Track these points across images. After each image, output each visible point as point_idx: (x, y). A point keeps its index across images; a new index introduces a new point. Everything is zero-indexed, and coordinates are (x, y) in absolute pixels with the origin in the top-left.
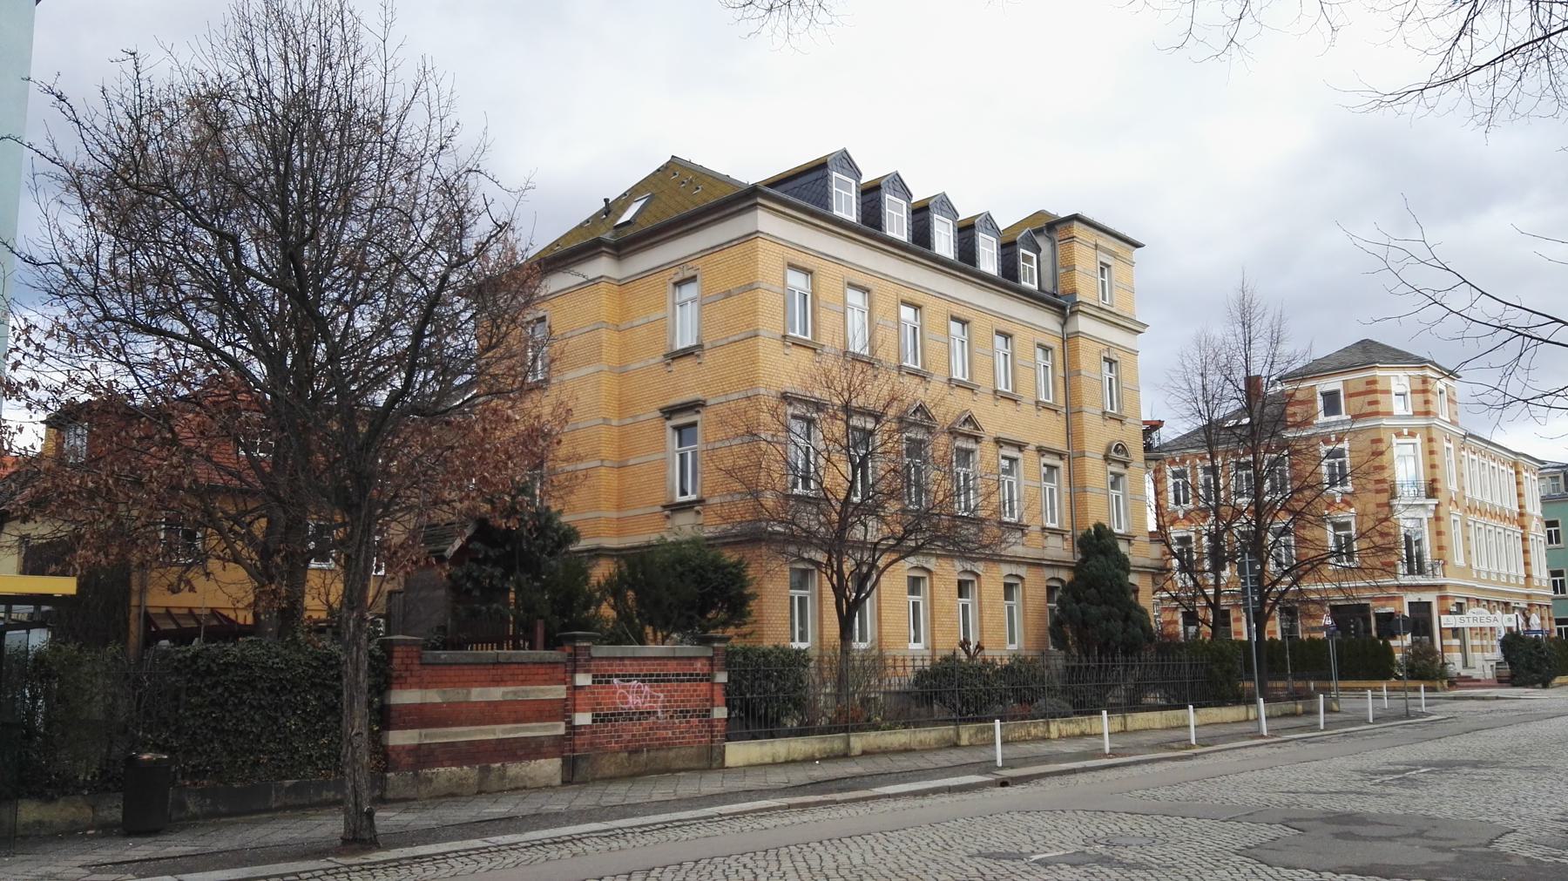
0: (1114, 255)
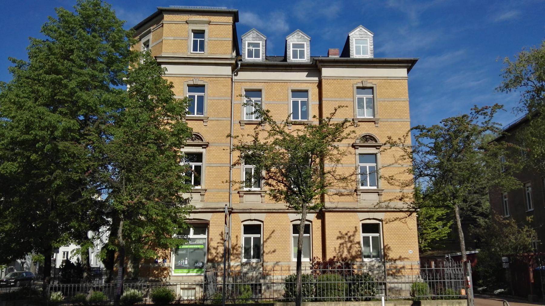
0: (209, 23)
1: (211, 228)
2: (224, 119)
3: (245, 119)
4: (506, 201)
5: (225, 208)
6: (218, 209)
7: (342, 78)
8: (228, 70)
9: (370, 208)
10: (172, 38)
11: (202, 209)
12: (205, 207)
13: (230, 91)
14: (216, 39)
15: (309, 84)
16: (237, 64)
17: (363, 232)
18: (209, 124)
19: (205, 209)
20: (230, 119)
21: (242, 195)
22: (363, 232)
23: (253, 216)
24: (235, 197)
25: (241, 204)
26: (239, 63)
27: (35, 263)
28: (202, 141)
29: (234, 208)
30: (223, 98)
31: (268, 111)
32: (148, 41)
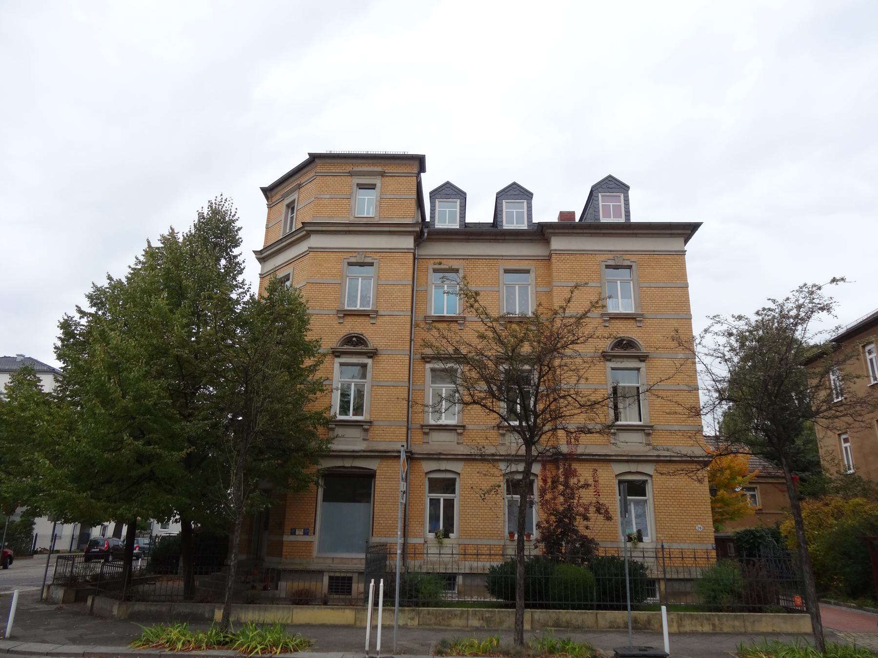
0: (383, 174)
1: (380, 486)
2: (401, 313)
3: (433, 314)
4: (846, 448)
5: (400, 452)
6: (388, 452)
7: (583, 252)
8: (408, 242)
9: (632, 456)
10: (328, 196)
11: (364, 451)
12: (370, 449)
13: (411, 271)
14: (392, 196)
15: (531, 262)
16: (422, 232)
17: (429, 493)
18: (380, 320)
19: (370, 451)
20: (410, 313)
21: (427, 431)
22: (429, 493)
23: (444, 466)
24: (417, 437)
25: (425, 446)
26: (426, 231)
27: (737, 341)
28: (367, 346)
29: (413, 451)
30: (400, 283)
31: (477, 294)
32: (294, 201)
